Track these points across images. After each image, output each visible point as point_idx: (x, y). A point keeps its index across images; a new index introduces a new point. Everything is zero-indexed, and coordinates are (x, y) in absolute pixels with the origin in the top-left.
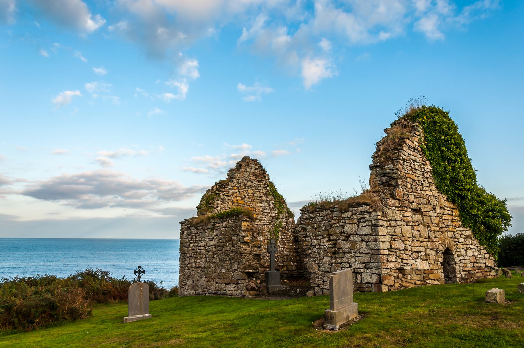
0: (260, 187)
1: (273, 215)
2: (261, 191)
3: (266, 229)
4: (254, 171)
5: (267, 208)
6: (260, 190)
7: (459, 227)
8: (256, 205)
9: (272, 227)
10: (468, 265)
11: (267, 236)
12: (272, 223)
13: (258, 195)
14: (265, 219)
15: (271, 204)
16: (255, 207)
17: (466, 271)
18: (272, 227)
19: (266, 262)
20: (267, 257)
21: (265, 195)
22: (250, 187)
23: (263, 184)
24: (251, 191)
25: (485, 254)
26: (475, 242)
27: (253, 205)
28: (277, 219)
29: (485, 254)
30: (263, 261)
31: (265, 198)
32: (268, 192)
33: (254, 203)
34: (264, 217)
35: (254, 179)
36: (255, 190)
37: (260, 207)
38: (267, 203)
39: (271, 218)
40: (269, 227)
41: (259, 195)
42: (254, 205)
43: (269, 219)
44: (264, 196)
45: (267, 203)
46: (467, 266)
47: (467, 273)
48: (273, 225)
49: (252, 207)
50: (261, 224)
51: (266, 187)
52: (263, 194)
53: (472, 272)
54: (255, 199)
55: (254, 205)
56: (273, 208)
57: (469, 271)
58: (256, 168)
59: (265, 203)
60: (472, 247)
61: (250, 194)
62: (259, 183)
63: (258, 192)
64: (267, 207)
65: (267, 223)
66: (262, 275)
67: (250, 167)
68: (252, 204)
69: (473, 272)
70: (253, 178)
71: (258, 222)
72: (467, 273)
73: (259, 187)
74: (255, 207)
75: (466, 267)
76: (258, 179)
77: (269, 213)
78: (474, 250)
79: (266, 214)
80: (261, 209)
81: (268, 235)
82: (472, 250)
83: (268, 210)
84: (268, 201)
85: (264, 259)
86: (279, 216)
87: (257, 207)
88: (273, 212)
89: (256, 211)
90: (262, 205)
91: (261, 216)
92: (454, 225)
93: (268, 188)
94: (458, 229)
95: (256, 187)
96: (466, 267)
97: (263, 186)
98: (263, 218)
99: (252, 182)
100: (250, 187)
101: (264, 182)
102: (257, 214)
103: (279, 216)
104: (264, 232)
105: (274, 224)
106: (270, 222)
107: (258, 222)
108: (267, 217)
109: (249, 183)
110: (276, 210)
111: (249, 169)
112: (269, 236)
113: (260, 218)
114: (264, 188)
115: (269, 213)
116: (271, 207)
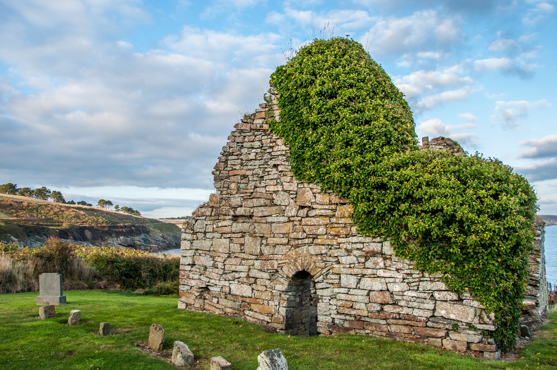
47: (353, 318)
69: (373, 321)
82: (383, 280)
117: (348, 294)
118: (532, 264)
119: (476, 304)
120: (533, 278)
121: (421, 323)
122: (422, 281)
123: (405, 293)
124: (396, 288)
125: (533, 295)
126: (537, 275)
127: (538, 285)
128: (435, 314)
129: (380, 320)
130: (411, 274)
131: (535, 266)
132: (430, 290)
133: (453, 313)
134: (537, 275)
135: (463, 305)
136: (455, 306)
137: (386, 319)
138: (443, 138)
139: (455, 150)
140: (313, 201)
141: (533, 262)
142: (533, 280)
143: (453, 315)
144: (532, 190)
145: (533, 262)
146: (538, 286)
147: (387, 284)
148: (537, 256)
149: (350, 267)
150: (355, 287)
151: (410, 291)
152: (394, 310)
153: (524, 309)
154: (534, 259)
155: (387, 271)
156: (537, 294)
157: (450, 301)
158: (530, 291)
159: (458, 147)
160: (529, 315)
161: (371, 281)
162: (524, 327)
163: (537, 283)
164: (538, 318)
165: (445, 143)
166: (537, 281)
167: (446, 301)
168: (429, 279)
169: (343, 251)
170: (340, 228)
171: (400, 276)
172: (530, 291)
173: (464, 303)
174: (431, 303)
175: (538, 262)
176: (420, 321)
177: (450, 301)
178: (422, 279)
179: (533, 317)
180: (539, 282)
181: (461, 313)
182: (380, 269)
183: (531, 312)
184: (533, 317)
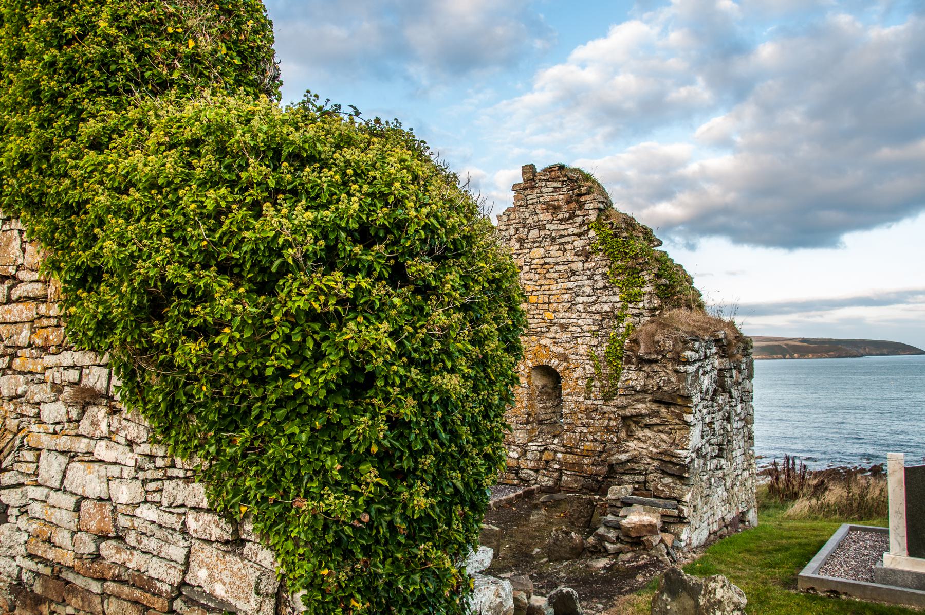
0: (569, 235)
1: (606, 308)
2: (568, 247)
3: (582, 349)
4: (548, 198)
5: (584, 292)
6: (568, 243)
7: (61, 348)
8: (552, 287)
9: (600, 344)
10: (62, 537)
11: (585, 369)
12: (603, 332)
13: (558, 260)
14: (580, 322)
15: (596, 277)
16: (547, 293)
17: (45, 561)
18: (600, 344)
19: (580, 440)
20: (584, 426)
21: (578, 256)
22: (537, 242)
23: (576, 225)
24: (538, 252)
25: (197, 509)
26: (132, 431)
27: (543, 288)
28: (620, 318)
29: (197, 509)
30: (570, 438)
31: (580, 265)
32: (589, 244)
33: (547, 282)
34: (574, 316)
35: (550, 218)
36: (552, 248)
37: (564, 291)
38: (586, 277)
39: (597, 317)
40: (592, 343)
41: (561, 259)
42: (546, 287)
43: (590, 322)
44: (576, 258)
45: (586, 277)
46: (57, 540)
47: (47, 571)
48: (603, 336)
49: (538, 293)
50: (566, 336)
51: (586, 233)
52: (576, 254)
53: (71, 577)
54: (548, 271)
55: (546, 287)
56: (605, 288)
57: (57, 569)
58: (555, 188)
59: (579, 278)
60: (102, 450)
61: (534, 262)
62: (562, 227)
63: (560, 250)
64: (585, 289)
65: (586, 334)
66: (568, 472)
67: (537, 190)
68: (541, 286)
69: (79, 582)
70: (544, 216)
71: (556, 332)
72: (47, 571)
73: (561, 237)
74: (547, 293)
75: (49, 541)
76: (560, 216)
77: (594, 303)
78: (114, 471)
79: (580, 307)
80: (566, 297)
81: (587, 367)
82: (102, 470)
83: (589, 296)
84: (588, 269)
85: (574, 432)
86: (624, 308)
87: (554, 292)
88: (605, 299)
89: (550, 303)
90: (569, 285)
91: (567, 314)
92: (39, 342)
93: (592, 233)
94: (49, 360)
95: (553, 240)
96: (49, 541)
97: (576, 231)
98: (571, 321)
99: (542, 228)
100: (537, 242)
101: (580, 219)
102: (554, 312)
103: (624, 308)
104: (573, 357)
105: (607, 334)
106: (593, 328)
107: (556, 332)
108: (584, 315)
109: (534, 233)
110: (614, 294)
111: (534, 196)
112: (590, 369)
113: (562, 321)
114: (579, 235)
115: (594, 303)
116: (600, 284)
117: (45, 502)
118: (676, 427)
119: (266, 557)
120: (674, 460)
121: (161, 600)
122: (170, 478)
123: (138, 512)
124: (124, 493)
125: (674, 499)
126: (684, 453)
127: (686, 475)
128: (187, 580)
129: (91, 581)
130: (152, 457)
131: (683, 432)
132: (183, 506)
133: (221, 580)
134: (684, 453)
135: (242, 556)
136: (227, 558)
137: (103, 580)
138: (562, 167)
139: (583, 190)
140: (20, 261)
141: (677, 424)
142: (675, 464)
143: (222, 586)
144: (427, 154)
145: (677, 424)
146: (687, 478)
147: (108, 480)
148: (685, 409)
149: (55, 433)
150: (58, 486)
151: (148, 505)
152: (118, 556)
153: (633, 535)
154: (680, 417)
155: (112, 444)
156: (683, 495)
157: (217, 541)
158: (669, 488)
159: (589, 184)
160: (644, 549)
161: (84, 470)
162: (568, 592)
163: (685, 471)
164: (662, 556)
165: (566, 176)
166: (684, 466)
167: (208, 542)
168: (181, 474)
169: (47, 387)
170: (50, 329)
171: (129, 459)
172: (669, 488)
173: (246, 550)
174: (181, 544)
175: (686, 423)
176: (160, 595)
177: (217, 541)
178: (170, 472)
179: (653, 552)
180: (689, 469)
181: (238, 583)
182: (101, 438)
183: (648, 540)
184: (653, 552)
